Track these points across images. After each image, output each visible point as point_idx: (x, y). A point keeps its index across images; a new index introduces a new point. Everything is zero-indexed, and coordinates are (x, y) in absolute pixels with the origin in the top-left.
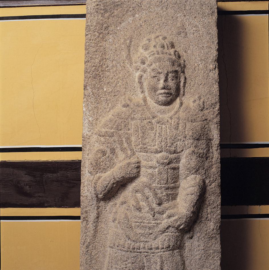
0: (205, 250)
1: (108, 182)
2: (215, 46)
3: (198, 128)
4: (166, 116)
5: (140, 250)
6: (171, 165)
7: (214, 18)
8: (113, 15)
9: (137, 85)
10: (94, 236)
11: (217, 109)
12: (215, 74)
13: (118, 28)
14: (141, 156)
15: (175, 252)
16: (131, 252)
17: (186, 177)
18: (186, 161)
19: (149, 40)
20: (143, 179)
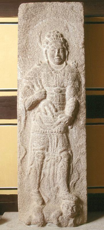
0: (79, 134)
1: (30, 101)
2: (82, 37)
3: (75, 76)
4: (59, 70)
5: (47, 133)
6: (62, 92)
7: (82, 23)
8: (32, 20)
9: (44, 55)
10: (24, 128)
11: (84, 67)
13: (35, 27)
14: (47, 88)
15: (64, 134)
16: (42, 134)
17: (69, 99)
18: (69, 91)
19: (50, 33)
20: (48, 99)
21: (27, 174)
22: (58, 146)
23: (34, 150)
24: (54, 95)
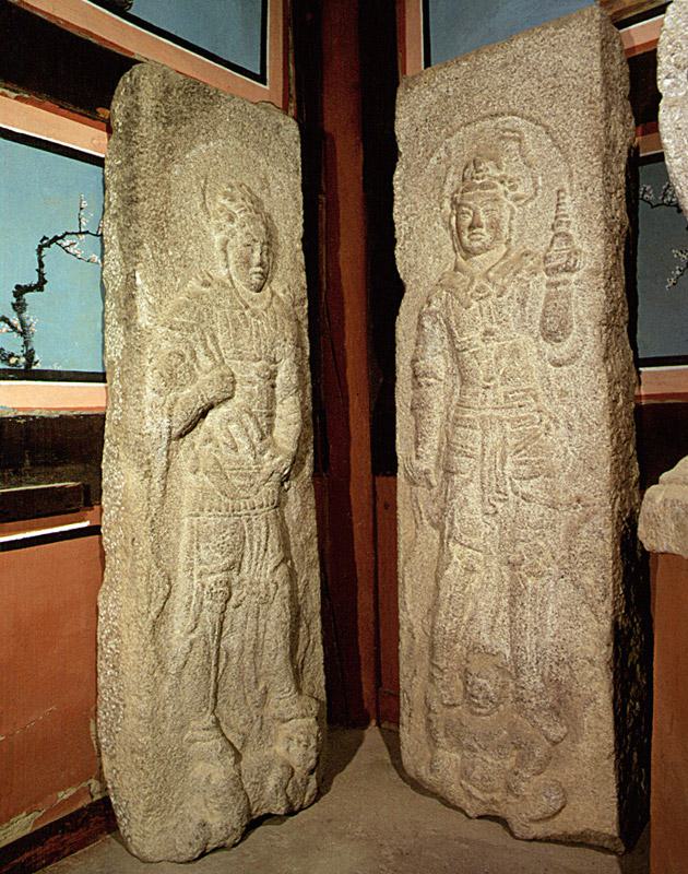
12: (301, 257)
14: (235, 365)
21: (172, 668)
22: (269, 550)
23: (200, 575)
24: (256, 387)
